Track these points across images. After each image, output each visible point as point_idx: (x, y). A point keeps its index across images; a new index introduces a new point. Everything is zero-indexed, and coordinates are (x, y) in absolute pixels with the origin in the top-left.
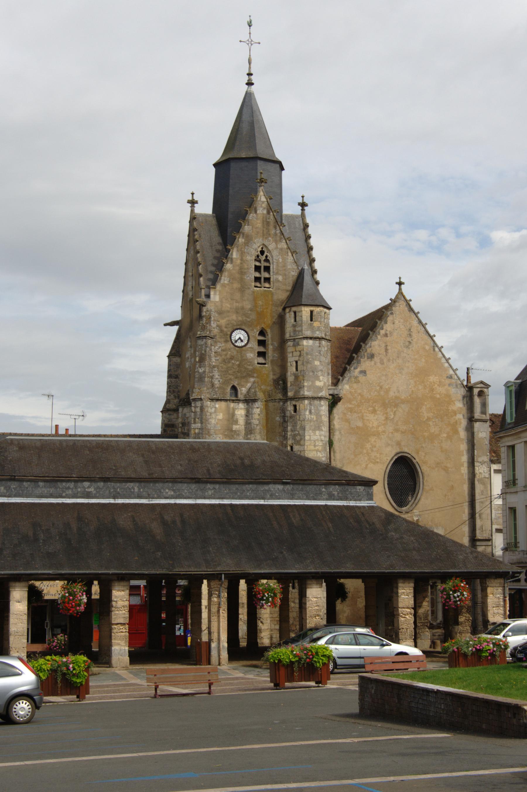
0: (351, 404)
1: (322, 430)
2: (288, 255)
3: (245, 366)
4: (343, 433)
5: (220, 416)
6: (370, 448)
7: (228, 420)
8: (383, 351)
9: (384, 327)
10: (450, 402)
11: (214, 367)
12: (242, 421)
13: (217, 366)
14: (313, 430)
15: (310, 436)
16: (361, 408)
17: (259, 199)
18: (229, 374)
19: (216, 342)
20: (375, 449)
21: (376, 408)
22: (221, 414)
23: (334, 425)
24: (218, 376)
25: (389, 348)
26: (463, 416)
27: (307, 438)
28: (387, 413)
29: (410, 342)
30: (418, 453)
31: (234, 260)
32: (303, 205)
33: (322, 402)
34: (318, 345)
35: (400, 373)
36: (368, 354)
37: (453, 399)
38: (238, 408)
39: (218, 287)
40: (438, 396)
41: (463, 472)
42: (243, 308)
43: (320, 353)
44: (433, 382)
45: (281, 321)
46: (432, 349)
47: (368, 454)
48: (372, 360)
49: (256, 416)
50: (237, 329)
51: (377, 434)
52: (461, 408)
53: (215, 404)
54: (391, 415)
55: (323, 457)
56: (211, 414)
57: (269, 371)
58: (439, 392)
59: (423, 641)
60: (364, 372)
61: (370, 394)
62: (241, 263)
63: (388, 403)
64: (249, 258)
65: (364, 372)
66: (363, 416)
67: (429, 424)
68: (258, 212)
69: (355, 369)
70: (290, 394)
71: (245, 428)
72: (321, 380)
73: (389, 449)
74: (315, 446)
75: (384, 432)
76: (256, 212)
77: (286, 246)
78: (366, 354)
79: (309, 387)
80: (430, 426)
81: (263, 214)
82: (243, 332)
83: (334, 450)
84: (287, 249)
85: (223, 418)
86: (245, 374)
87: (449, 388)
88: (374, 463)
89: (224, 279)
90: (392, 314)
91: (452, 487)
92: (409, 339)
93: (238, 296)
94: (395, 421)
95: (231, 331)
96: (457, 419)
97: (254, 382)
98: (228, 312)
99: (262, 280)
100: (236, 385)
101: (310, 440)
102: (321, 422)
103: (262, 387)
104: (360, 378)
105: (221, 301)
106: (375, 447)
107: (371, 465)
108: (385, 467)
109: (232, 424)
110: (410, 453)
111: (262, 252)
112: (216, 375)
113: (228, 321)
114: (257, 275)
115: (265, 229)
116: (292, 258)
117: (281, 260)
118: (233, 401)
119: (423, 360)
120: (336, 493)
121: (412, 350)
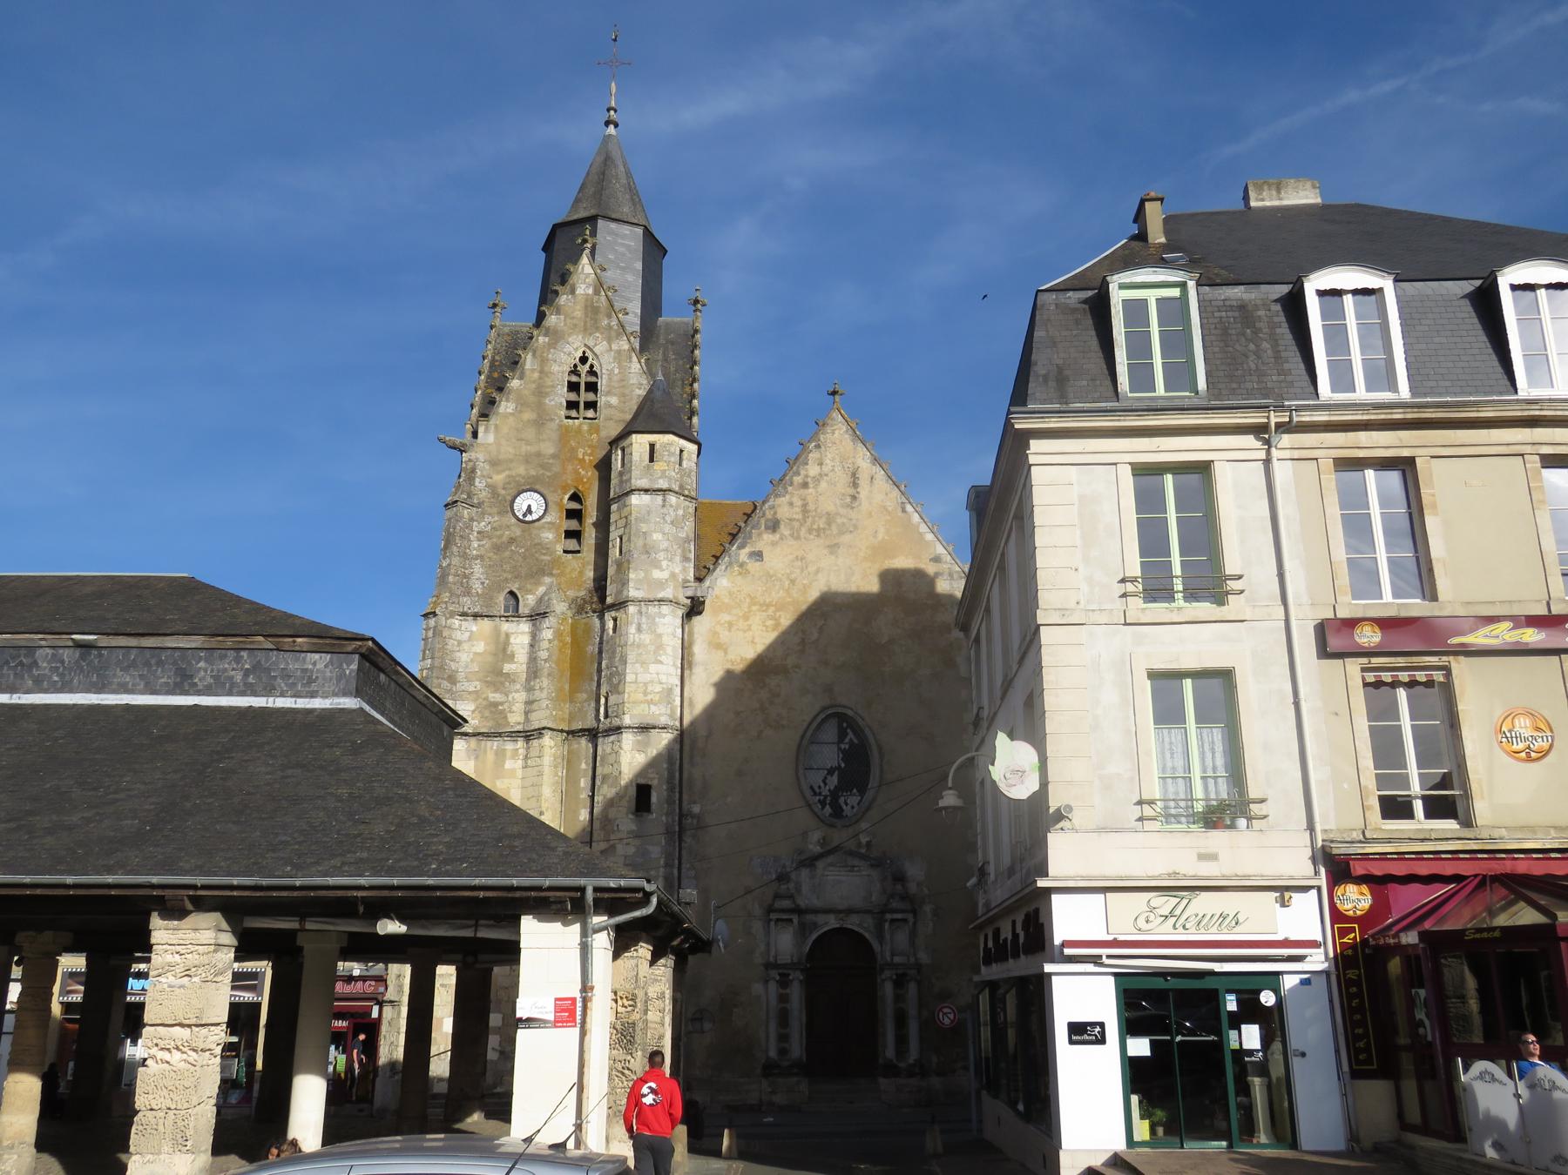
5: (480, 647)
12: (522, 656)
13: (481, 557)
19: (483, 514)
27: (629, 678)
29: (854, 498)
33: (665, 609)
39: (493, 420)
45: (604, 467)
49: (545, 645)
56: (460, 643)
57: (583, 567)
60: (758, 555)
64: (555, 368)
65: (758, 555)
69: (739, 548)
70: (609, 600)
74: (645, 694)
76: (573, 292)
77: (626, 347)
82: (536, 496)
89: (506, 407)
90: (818, 446)
93: (530, 433)
98: (511, 461)
99: (582, 405)
106: (778, 695)
111: (584, 360)
112: (478, 570)
114: (573, 397)
120: (239, 677)
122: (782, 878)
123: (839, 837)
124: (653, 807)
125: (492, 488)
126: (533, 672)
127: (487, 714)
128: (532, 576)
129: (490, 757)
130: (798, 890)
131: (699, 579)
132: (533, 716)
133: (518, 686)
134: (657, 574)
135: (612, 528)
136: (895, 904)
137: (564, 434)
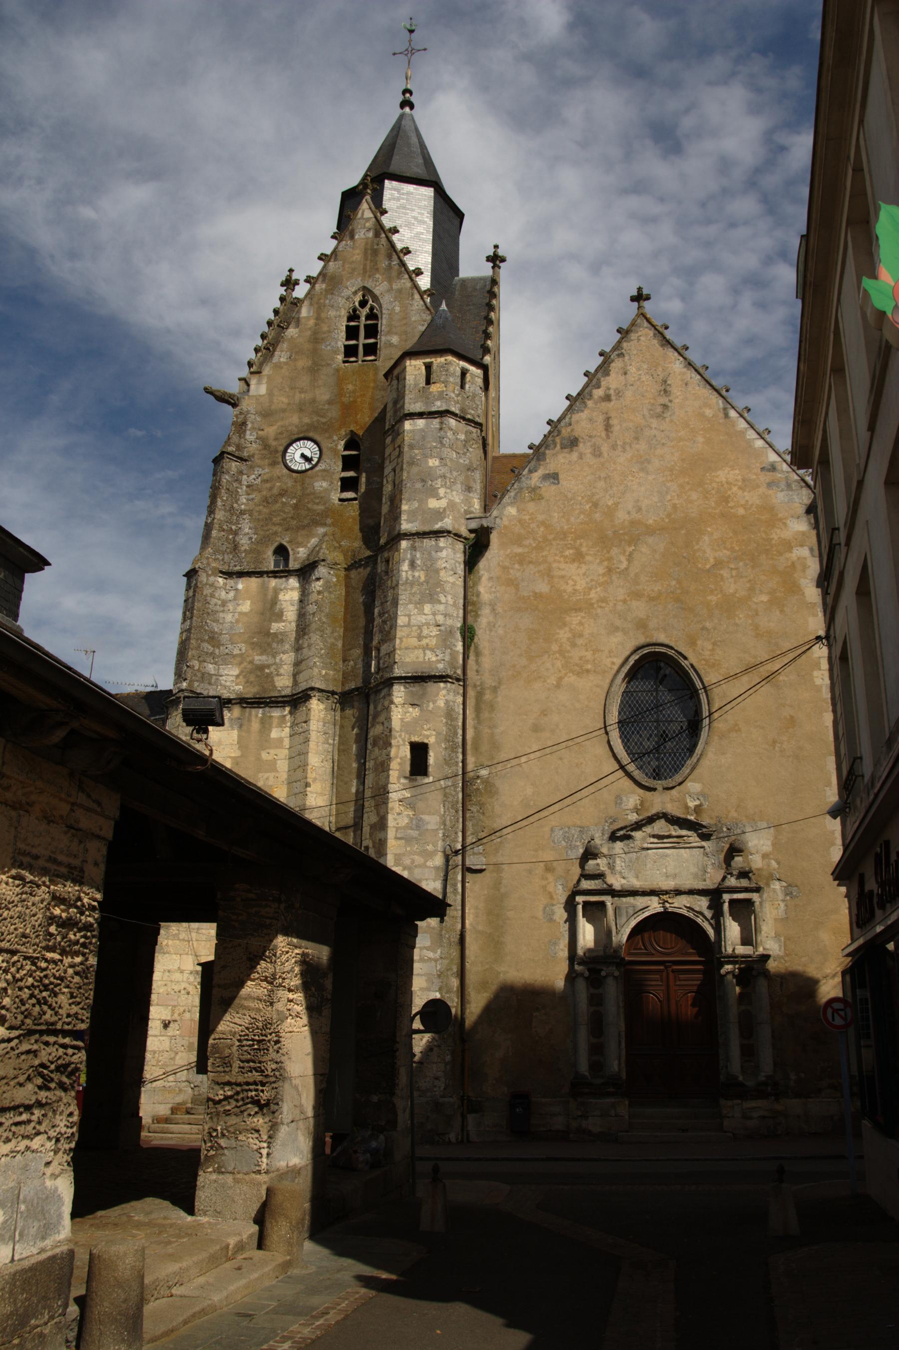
0: (520, 545)
1: (440, 602)
2: (413, 299)
3: (309, 506)
4: (499, 610)
5: (246, 606)
6: (568, 639)
7: (262, 614)
8: (601, 427)
9: (603, 383)
10: (773, 519)
11: (242, 513)
12: (291, 614)
13: (251, 512)
14: (416, 603)
15: (409, 616)
16: (544, 553)
17: (359, 215)
18: (274, 524)
20: (580, 641)
21: (584, 549)
22: (248, 602)
23: (478, 595)
24: (250, 528)
25: (614, 422)
26: (811, 550)
27: (401, 620)
28: (610, 559)
30: (693, 643)
31: (303, 321)
32: (495, 259)
34: (438, 426)
35: (642, 470)
36: (563, 438)
37: (780, 515)
38: (285, 588)
40: (741, 511)
41: (818, 682)
42: (314, 401)
43: (441, 443)
44: (727, 483)
46: (721, 415)
47: (562, 652)
48: (572, 451)
50: (299, 439)
51: (586, 607)
52: (803, 533)
53: (236, 583)
54: (620, 562)
55: (439, 661)
56: (224, 603)
58: (743, 502)
59: (229, 1179)
60: (554, 477)
61: (568, 520)
62: (316, 325)
63: (611, 537)
65: (554, 477)
66: (550, 569)
67: (722, 576)
68: (357, 237)
69: (530, 472)
71: (297, 626)
72: (442, 495)
73: (615, 639)
74: (420, 638)
75: (604, 600)
76: (352, 237)
78: (558, 440)
79: (413, 514)
80: (722, 579)
81: (367, 238)
82: (310, 444)
83: (476, 647)
84: (412, 288)
85: (251, 610)
86: (306, 522)
87: (771, 492)
88: (578, 674)
91: (792, 721)
92: (663, 400)
93: (304, 380)
94: (632, 575)
95: (285, 444)
96: (795, 559)
97: (325, 535)
98: (284, 411)
100: (285, 544)
101: (409, 625)
102: (439, 584)
103: (343, 543)
104: (543, 489)
105: (270, 393)
107: (571, 679)
108: (608, 681)
109: (270, 621)
110: (672, 644)
111: (363, 303)
112: (246, 527)
113: (282, 426)
115: (368, 262)
116: (422, 302)
117: (397, 309)
118: (275, 574)
119: (700, 439)
121: (671, 421)
122: (589, 854)
123: (660, 802)
124: (430, 769)
125: (264, 442)
126: (302, 628)
127: (252, 678)
128: (303, 527)
129: (255, 725)
130: (611, 867)
131: (486, 508)
132: (301, 678)
133: (287, 646)
134: (433, 503)
135: (387, 462)
136: (732, 882)
137: (340, 379)
